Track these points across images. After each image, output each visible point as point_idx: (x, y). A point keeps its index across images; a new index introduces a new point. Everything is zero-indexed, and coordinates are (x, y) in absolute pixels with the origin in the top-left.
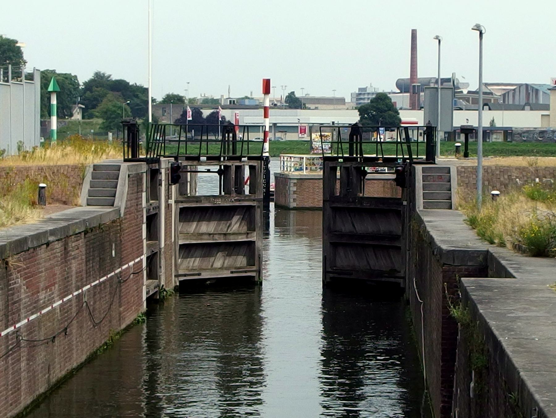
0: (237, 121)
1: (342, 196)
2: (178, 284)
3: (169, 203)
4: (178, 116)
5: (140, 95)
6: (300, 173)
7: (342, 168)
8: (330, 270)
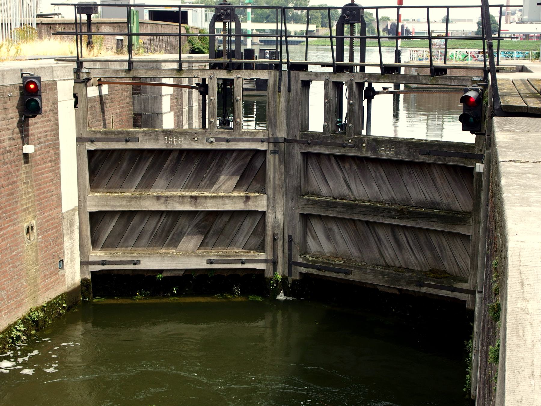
0: (413, 29)
1: (329, 134)
2: (89, 277)
3: (24, 152)
4: (385, 27)
5: (368, 16)
6: (421, 62)
7: (331, 85)
8: (300, 260)
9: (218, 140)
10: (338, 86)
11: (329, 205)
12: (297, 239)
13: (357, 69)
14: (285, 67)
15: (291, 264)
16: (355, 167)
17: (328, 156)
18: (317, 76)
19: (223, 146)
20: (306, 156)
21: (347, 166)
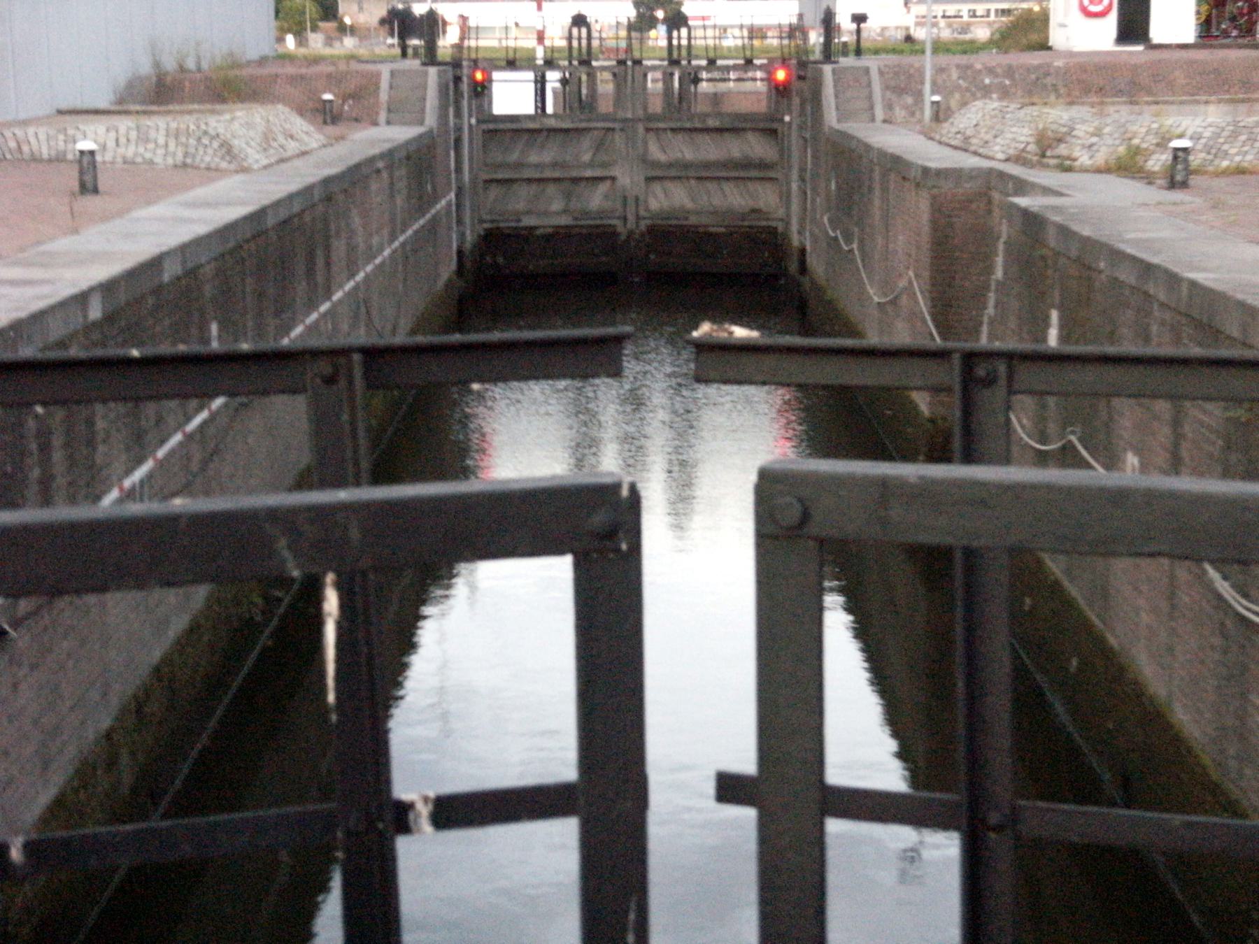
9: (581, 121)
10: (672, 74)
11: (670, 165)
12: (642, 198)
13: (684, 63)
14: (629, 63)
15: (638, 218)
16: (687, 138)
17: (665, 130)
18: (654, 68)
19: (584, 125)
20: (648, 130)
21: (680, 136)
